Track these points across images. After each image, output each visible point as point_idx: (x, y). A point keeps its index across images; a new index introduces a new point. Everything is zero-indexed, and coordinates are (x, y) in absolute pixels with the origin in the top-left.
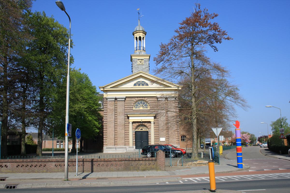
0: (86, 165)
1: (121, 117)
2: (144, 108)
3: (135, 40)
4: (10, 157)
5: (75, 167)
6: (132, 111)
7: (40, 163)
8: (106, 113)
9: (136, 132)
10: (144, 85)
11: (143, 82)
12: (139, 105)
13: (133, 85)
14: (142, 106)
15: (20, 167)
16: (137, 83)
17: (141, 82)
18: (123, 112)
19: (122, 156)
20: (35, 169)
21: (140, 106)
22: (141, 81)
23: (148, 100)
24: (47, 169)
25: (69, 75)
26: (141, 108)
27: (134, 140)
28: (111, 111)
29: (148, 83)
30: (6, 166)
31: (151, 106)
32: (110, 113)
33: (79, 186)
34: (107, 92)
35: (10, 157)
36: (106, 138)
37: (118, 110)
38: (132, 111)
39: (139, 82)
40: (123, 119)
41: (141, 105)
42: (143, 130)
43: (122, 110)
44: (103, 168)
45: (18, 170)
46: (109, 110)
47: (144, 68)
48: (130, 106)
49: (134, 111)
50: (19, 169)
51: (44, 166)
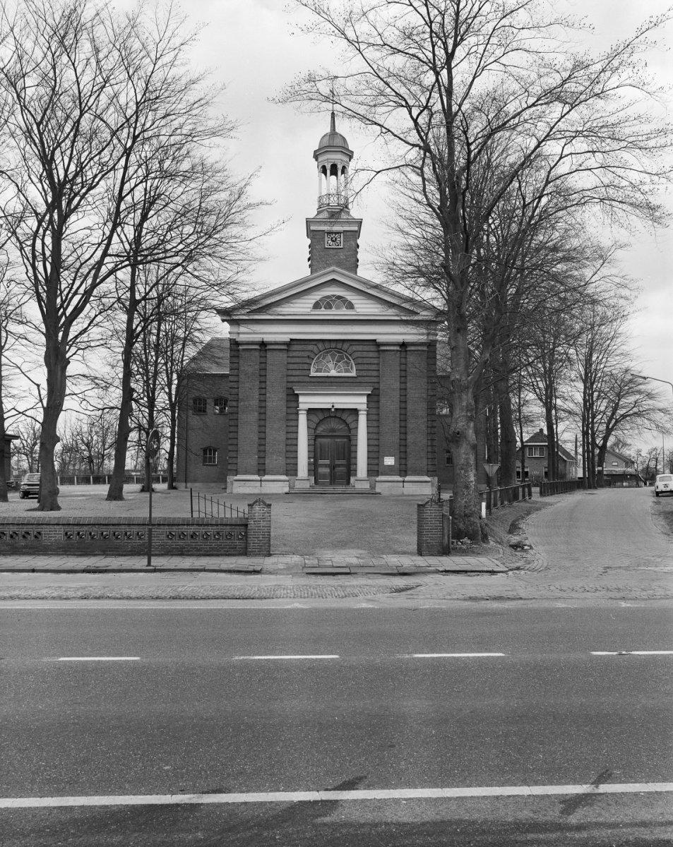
6: (308, 379)
13: (311, 306)
22: (334, 296)
23: (354, 348)
27: (312, 460)
29: (353, 302)
31: (360, 367)
34: (239, 325)
38: (308, 379)
39: (328, 297)
46: (242, 376)
49: (312, 380)
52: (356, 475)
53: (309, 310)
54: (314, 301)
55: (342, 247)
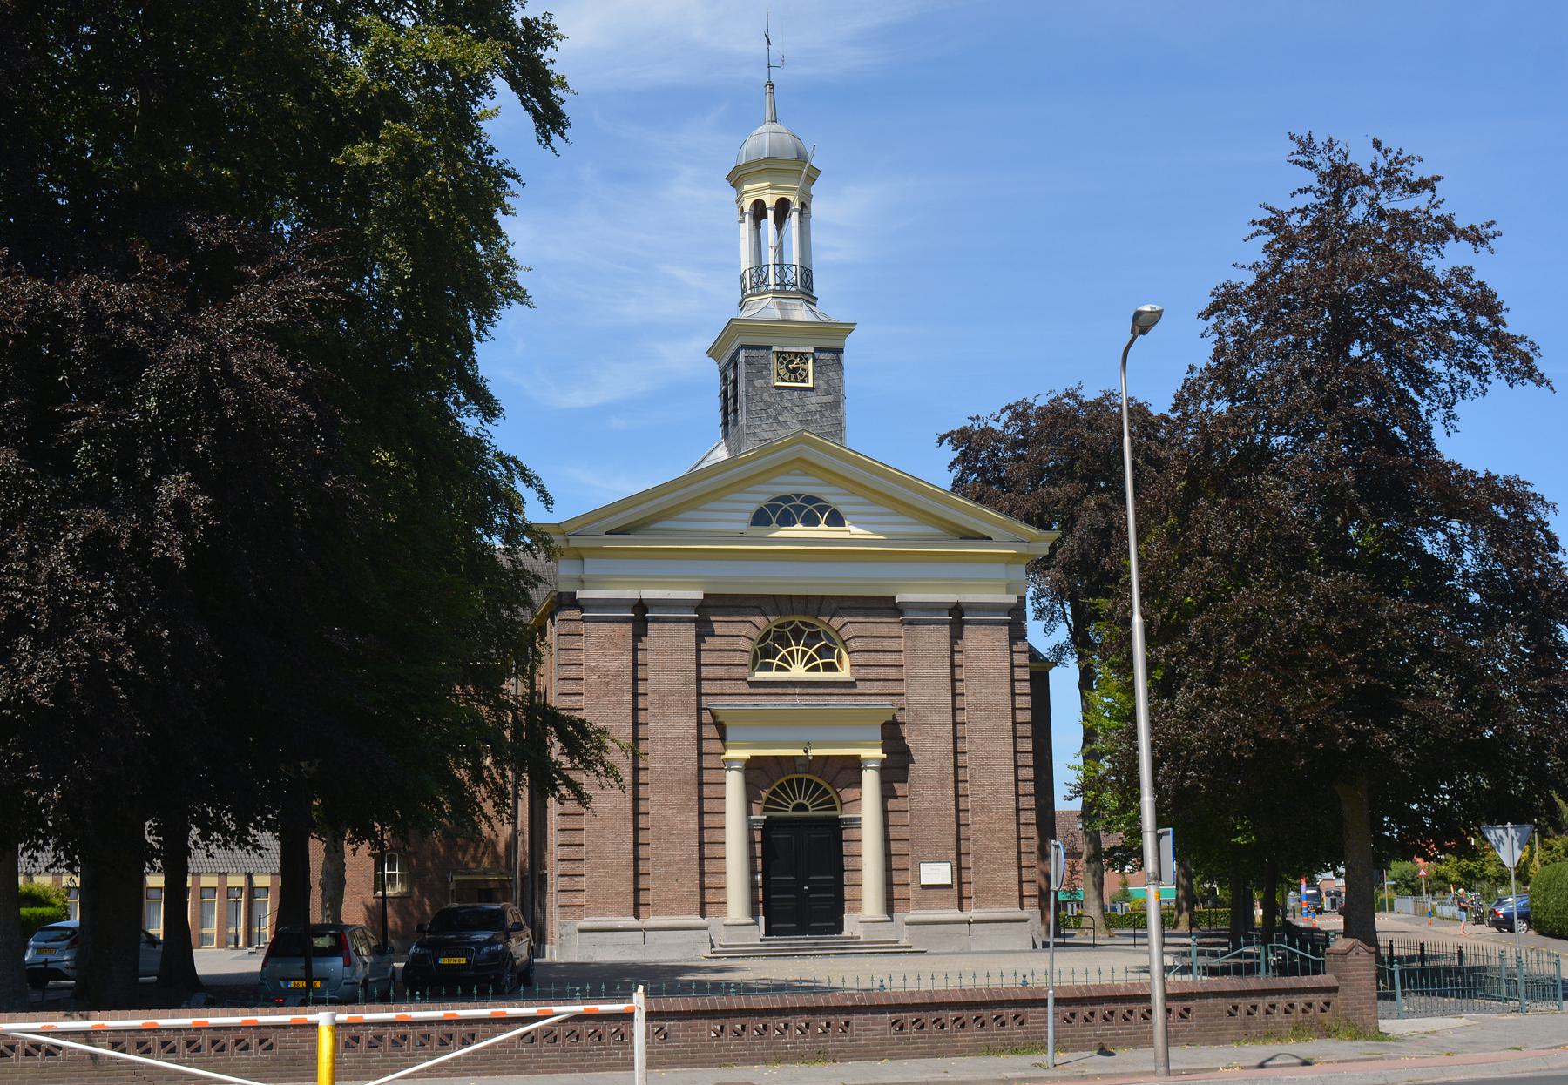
0: (1031, 1018)
1: (673, 725)
2: (816, 669)
3: (746, 228)
4: (588, 988)
5: (604, 1044)
7: (1270, 999)
8: (574, 698)
9: (769, 826)
10: (816, 523)
11: (810, 499)
12: (784, 652)
13: (748, 517)
14: (804, 654)
15: (1079, 1021)
16: (773, 507)
17: (798, 503)
18: (687, 695)
19: (1100, 972)
20: (801, 1043)
21: (791, 653)
22: (798, 496)
24: (856, 1040)
25: (1144, 616)
26: (798, 672)
28: (612, 686)
29: (842, 509)
30: (238, 1042)
32: (604, 702)
33: (1561, 1068)
35: (588, 988)
36: (577, 864)
37: (649, 681)
39: (786, 499)
40: (686, 738)
41: (794, 648)
42: (811, 813)
43: (682, 679)
44: (1108, 1029)
45: (720, 1051)
47: (812, 408)
48: (726, 654)
50: (722, 1045)
51: (1268, 1013)
52: (859, 909)
53: (743, 527)
54: (754, 507)
55: (810, 384)
